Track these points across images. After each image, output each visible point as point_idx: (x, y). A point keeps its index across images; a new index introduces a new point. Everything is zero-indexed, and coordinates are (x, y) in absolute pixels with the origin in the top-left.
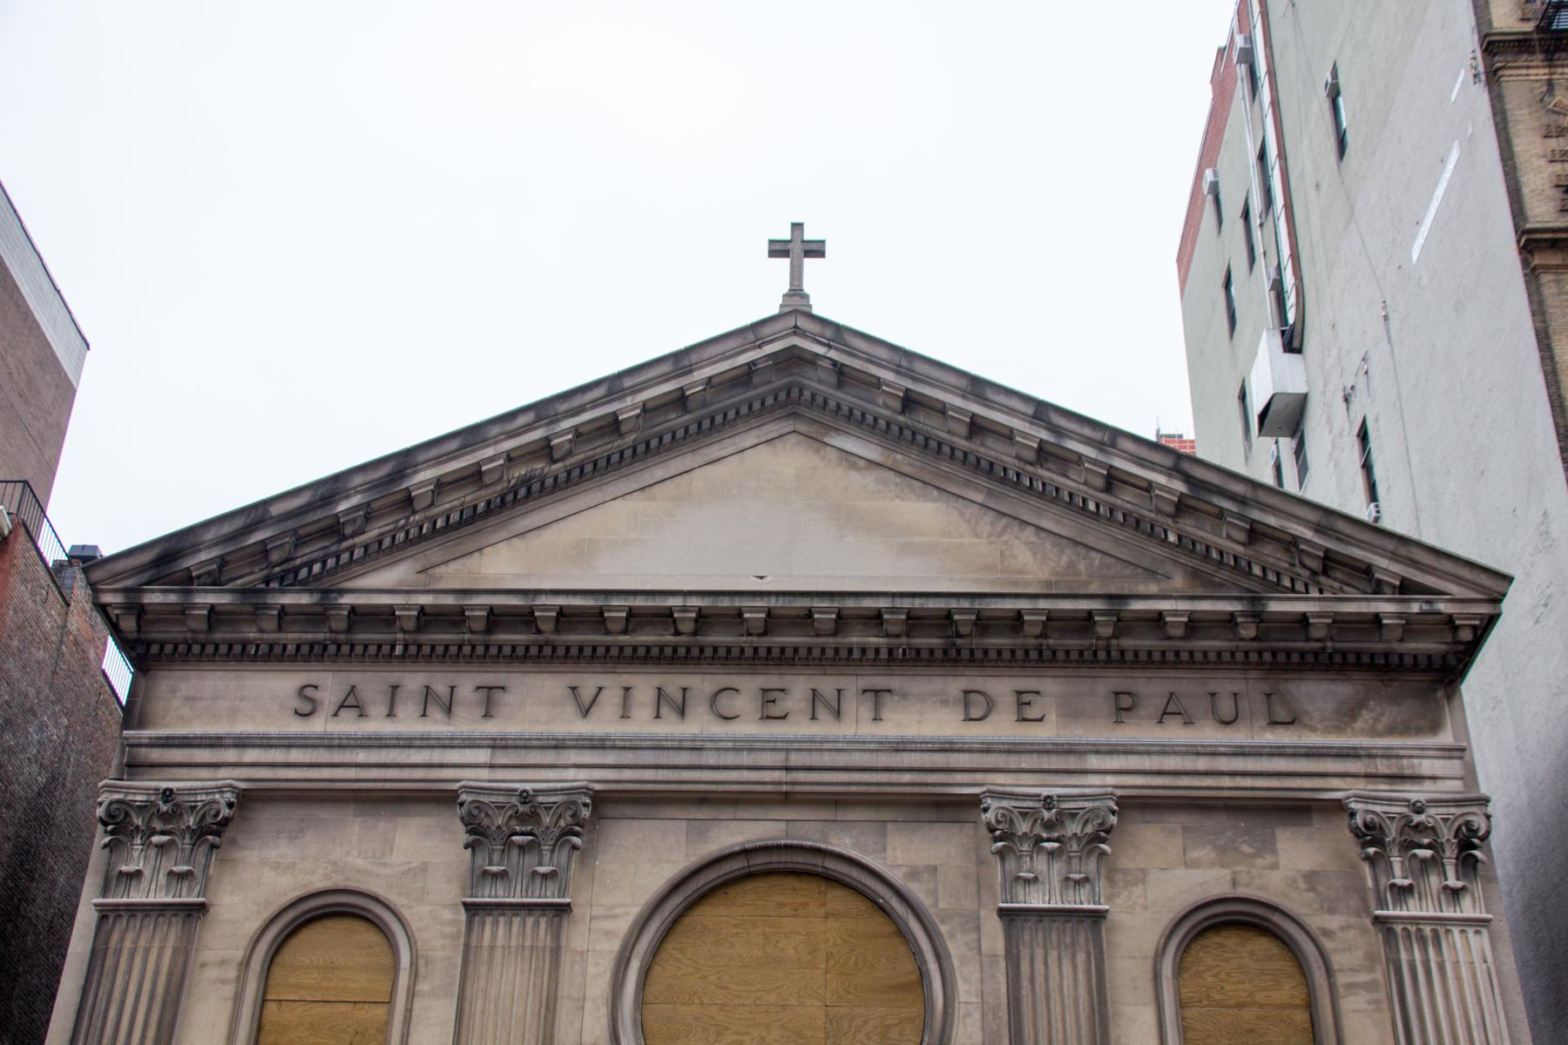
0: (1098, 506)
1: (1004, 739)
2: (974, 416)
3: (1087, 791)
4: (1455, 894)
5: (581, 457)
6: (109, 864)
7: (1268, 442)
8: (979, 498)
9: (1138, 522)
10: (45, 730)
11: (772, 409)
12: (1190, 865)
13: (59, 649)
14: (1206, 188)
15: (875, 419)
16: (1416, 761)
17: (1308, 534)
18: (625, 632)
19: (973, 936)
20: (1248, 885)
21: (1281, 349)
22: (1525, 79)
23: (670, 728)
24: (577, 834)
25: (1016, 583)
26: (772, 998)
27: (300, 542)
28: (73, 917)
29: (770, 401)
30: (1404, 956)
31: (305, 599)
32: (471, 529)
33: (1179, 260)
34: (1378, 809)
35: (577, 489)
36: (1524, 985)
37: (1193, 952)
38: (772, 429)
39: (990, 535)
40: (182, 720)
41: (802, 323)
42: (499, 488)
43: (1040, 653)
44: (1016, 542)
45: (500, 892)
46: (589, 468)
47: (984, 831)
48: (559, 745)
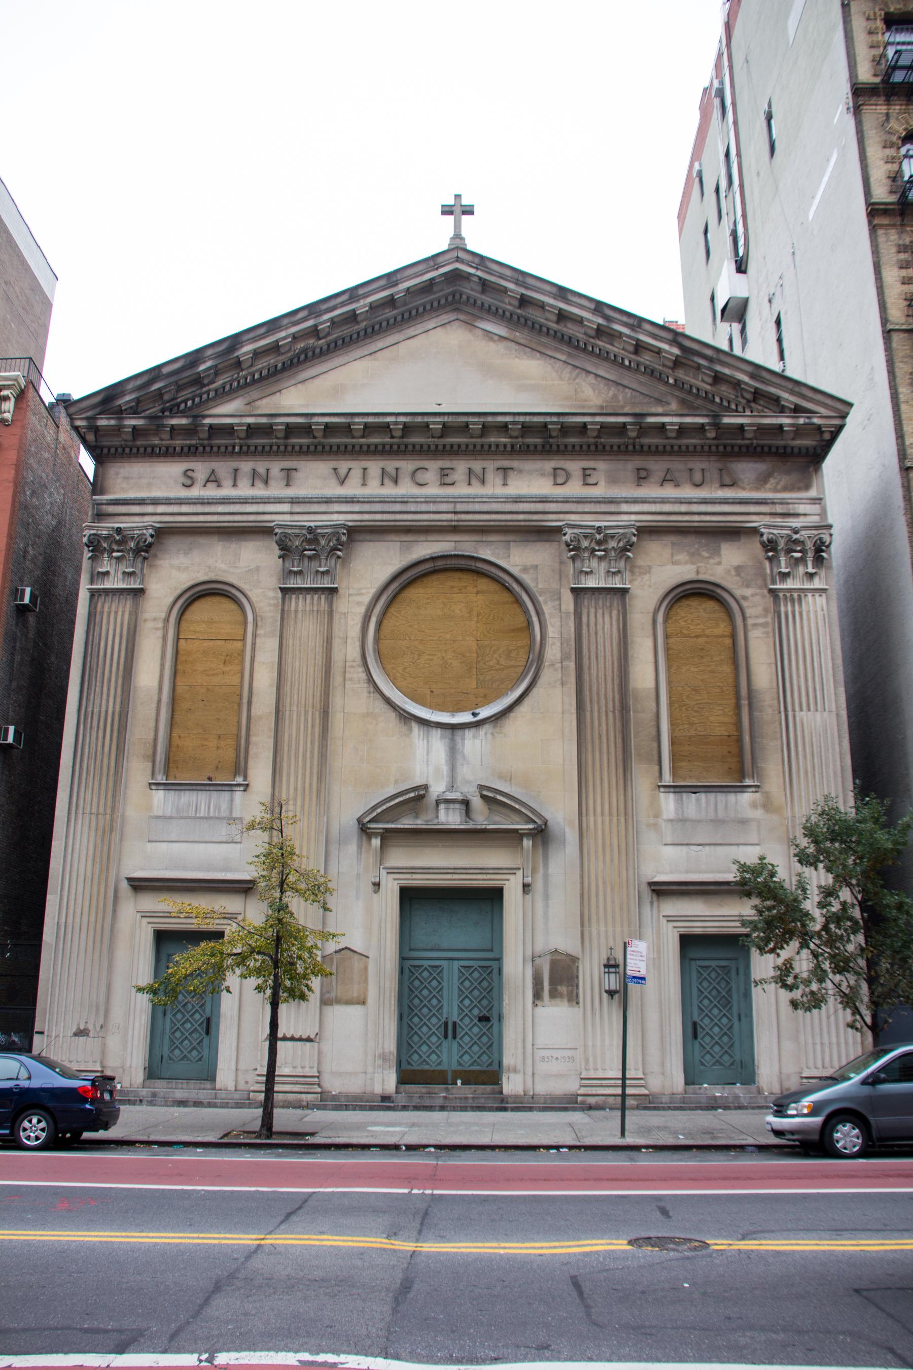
0: (630, 362)
1: (575, 495)
2: (560, 310)
3: (620, 524)
4: (811, 576)
5: (335, 336)
6: (92, 568)
7: (726, 325)
8: (563, 358)
9: (652, 371)
10: (54, 496)
11: (444, 307)
12: (674, 563)
13: (56, 452)
14: (695, 173)
15: (504, 312)
16: (796, 506)
17: (746, 379)
18: (363, 437)
19: (557, 603)
20: (705, 573)
21: (735, 271)
22: (875, 111)
23: (389, 491)
24: (340, 550)
25: (583, 407)
26: (448, 636)
27: (180, 388)
28: (77, 595)
29: (443, 301)
30: (783, 609)
31: (184, 421)
32: (274, 379)
33: (679, 217)
34: (775, 532)
35: (333, 355)
36: (840, 621)
37: (674, 609)
38: (445, 318)
39: (569, 379)
40: (123, 490)
41: (461, 255)
42: (289, 355)
43: (596, 446)
44: (584, 383)
45: (299, 582)
46: (340, 342)
47: (564, 546)
48: (328, 501)
